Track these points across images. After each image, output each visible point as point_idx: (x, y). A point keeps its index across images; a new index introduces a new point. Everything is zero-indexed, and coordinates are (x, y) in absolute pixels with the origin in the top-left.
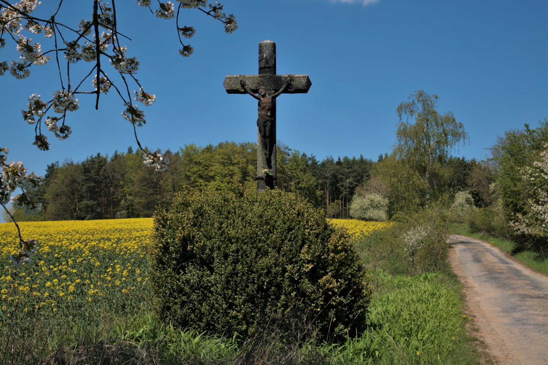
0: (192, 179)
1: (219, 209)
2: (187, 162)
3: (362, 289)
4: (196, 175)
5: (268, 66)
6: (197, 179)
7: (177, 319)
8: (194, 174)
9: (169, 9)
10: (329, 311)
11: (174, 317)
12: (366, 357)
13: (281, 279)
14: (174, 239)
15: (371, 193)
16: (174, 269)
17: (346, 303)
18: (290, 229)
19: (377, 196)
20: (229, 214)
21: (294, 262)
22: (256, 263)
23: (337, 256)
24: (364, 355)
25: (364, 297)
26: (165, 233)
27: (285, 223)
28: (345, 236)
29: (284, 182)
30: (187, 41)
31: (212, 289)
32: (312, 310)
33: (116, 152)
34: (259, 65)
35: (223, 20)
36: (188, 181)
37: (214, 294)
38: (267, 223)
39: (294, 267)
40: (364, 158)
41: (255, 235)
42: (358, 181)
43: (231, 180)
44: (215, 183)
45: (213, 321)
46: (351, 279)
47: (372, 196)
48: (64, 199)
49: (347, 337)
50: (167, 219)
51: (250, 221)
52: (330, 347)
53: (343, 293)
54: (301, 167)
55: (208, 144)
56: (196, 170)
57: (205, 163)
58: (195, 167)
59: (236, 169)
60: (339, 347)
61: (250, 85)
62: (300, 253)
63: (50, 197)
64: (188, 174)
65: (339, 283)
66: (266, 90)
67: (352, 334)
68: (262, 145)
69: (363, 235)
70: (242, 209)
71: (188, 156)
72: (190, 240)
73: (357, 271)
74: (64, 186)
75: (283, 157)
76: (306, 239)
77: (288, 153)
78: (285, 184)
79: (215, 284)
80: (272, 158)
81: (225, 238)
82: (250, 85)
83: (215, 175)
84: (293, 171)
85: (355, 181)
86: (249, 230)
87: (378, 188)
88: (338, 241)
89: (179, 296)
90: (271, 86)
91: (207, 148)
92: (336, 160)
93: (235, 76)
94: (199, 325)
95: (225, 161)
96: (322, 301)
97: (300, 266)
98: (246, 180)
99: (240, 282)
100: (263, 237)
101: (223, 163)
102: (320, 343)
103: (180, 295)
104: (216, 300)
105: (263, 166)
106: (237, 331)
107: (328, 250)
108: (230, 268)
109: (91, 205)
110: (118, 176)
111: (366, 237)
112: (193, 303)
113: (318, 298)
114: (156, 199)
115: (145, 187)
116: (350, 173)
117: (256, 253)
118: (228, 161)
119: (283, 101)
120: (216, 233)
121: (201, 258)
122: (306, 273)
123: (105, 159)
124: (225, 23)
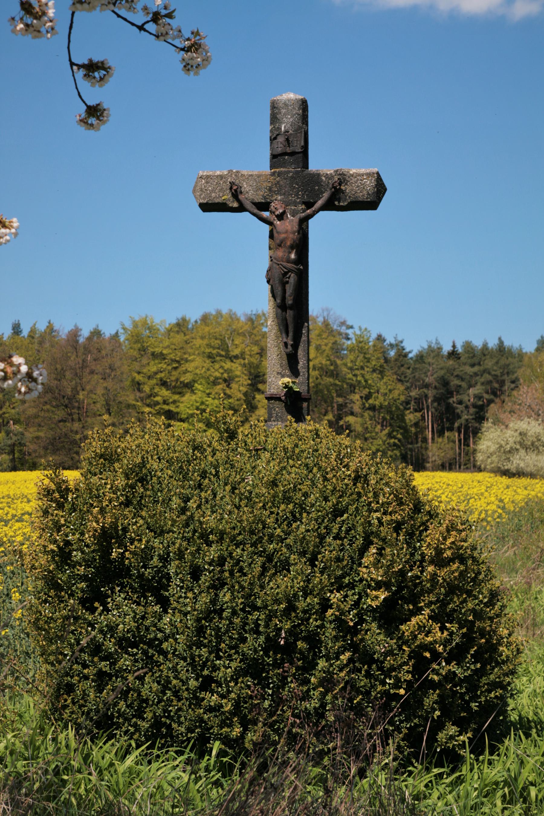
0: (147, 389)
1: (181, 467)
2: (135, 353)
3: (499, 643)
4: (154, 381)
5: (291, 150)
7: (88, 713)
8: (149, 378)
9: (44, 13)
10: (425, 694)
11: (81, 706)
12: (508, 801)
13: (319, 623)
14: (82, 534)
15: (520, 419)
16: (83, 602)
17: (462, 676)
18: (337, 512)
19: (533, 423)
20: (204, 478)
21: (347, 585)
22: (262, 587)
23: (443, 573)
24: (504, 796)
25: (504, 662)
26: (62, 521)
27: (326, 499)
28: (460, 527)
29: (339, 396)
30: (94, 94)
31: (165, 645)
32: (386, 693)
34: (272, 149)
35: (177, 42)
36: (138, 394)
37: (170, 656)
38: (287, 499)
39: (346, 596)
40: (507, 343)
41: (260, 526)
42: (494, 394)
44: (194, 397)
45: (167, 717)
46: (473, 623)
47: (523, 425)
49: (466, 753)
50: (68, 490)
51: (251, 493)
52: (427, 778)
53: (457, 655)
54: (374, 363)
55: (180, 316)
56: (154, 369)
59: (237, 368)
60: (449, 775)
61: (250, 193)
62: (360, 565)
64: (138, 378)
65: (446, 633)
66: (287, 204)
67: (477, 749)
68: (279, 325)
69: (503, 508)
70: (232, 466)
71: (137, 342)
72: (118, 537)
73: (486, 605)
75: (335, 343)
76: (372, 533)
77: (347, 334)
78: (340, 400)
79: (173, 636)
80: (301, 353)
81: (195, 531)
82: (250, 193)
83: (194, 381)
84: (358, 372)
85: (487, 392)
86: (247, 515)
87: (536, 408)
88: (445, 539)
89: (92, 661)
90: (297, 195)
91: (178, 325)
92: (447, 348)
93: (218, 173)
94: (135, 725)
96: (408, 672)
97: (359, 594)
99: (227, 631)
100: (279, 530)
101: (210, 356)
102: (405, 767)
103: (96, 659)
104: (174, 669)
105: (280, 370)
106: (220, 739)
107: (423, 560)
108: (205, 599)
111: (508, 513)
112: (122, 677)
113: (401, 666)
114: (72, 431)
115: (48, 407)
116: (476, 374)
117: (263, 566)
118: (220, 352)
119: (325, 228)
120: (174, 521)
121: (141, 576)
122: (373, 610)
124: (182, 49)
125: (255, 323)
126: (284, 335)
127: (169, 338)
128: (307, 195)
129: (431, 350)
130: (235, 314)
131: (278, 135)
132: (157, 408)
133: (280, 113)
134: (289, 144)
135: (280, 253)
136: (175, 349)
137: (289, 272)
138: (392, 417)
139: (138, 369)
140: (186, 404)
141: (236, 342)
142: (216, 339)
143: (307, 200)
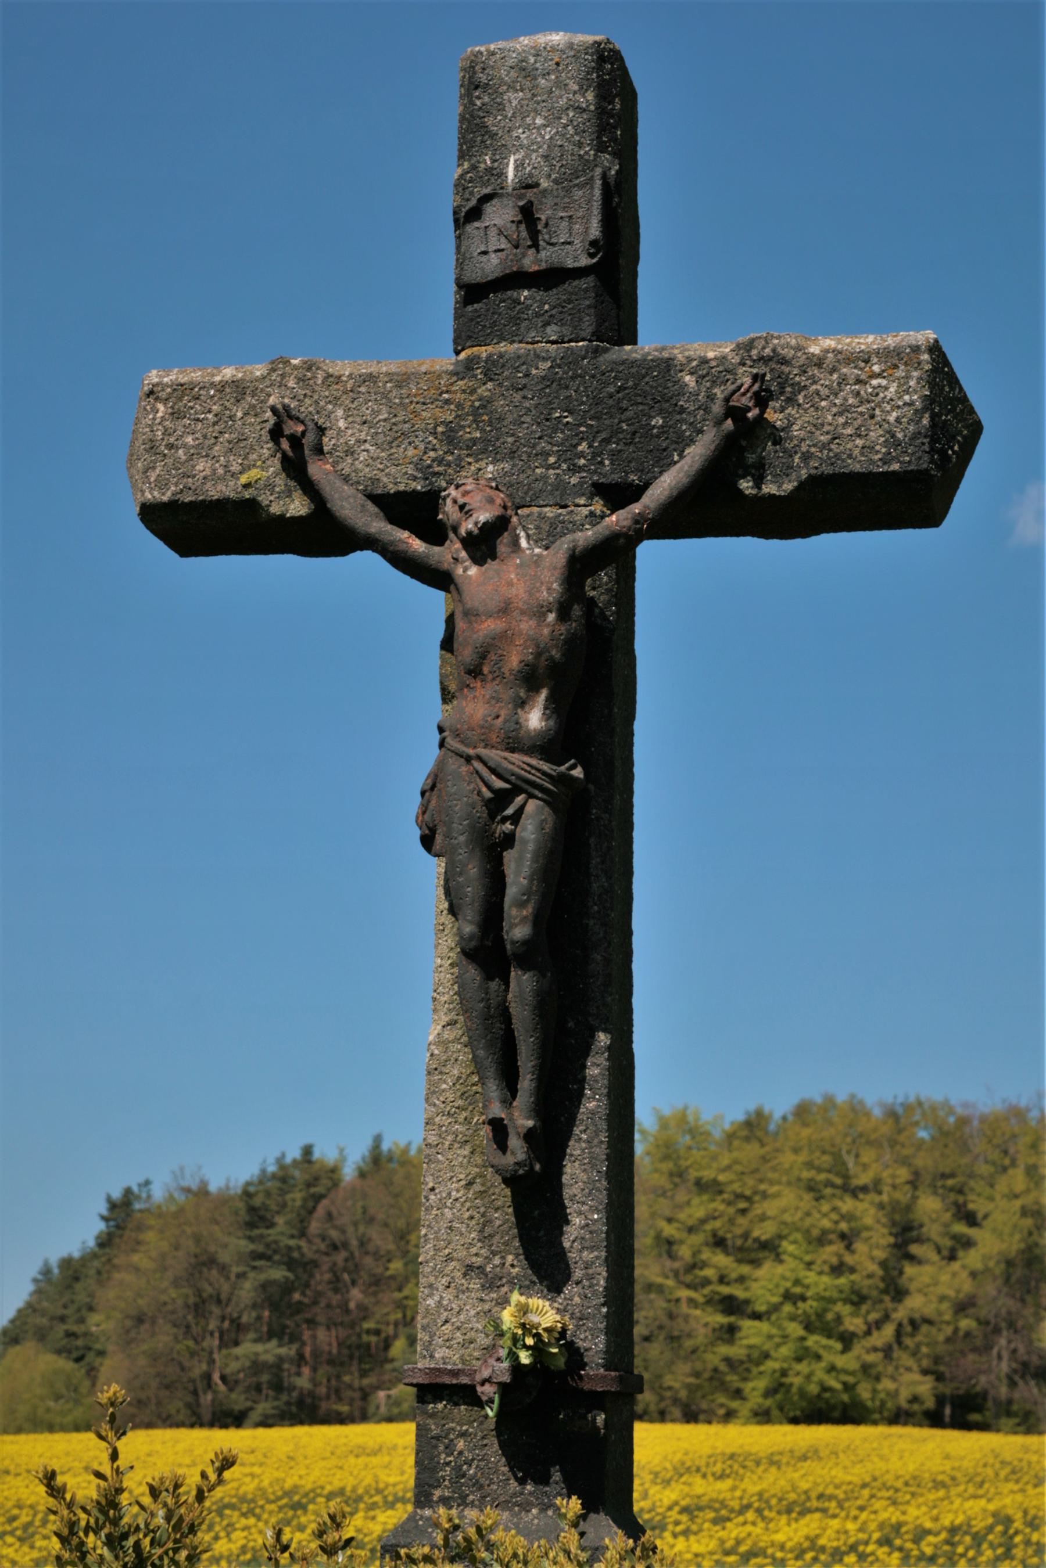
0: (685, 1252)
2: (662, 1181)
5: (564, 276)
6: (706, 1255)
8: (691, 1230)
33: (378, 1140)
36: (668, 1263)
43: (849, 1259)
44: (780, 1269)
48: (164, 1337)
55: (752, 1107)
56: (700, 1213)
57: (736, 1187)
58: (696, 1201)
61: (361, 457)
63: (109, 1326)
64: (669, 1230)
71: (666, 1157)
74: (165, 1284)
82: (361, 457)
83: (781, 1237)
90: (568, 453)
95: (822, 1177)
98: (911, 1258)
101: (811, 1187)
109: (270, 1358)
110: (382, 1240)
123: (334, 1171)
125: (903, 1121)
126: (494, 1089)
127: (730, 1151)
128: (613, 454)
130: (861, 1103)
131: (487, 198)
132: (706, 1291)
133: (501, 107)
134: (534, 234)
135: (477, 707)
136: (743, 1173)
137: (516, 790)
139: (667, 1213)
140: (764, 1283)
141: (864, 1159)
142: (824, 1152)
143: (616, 478)
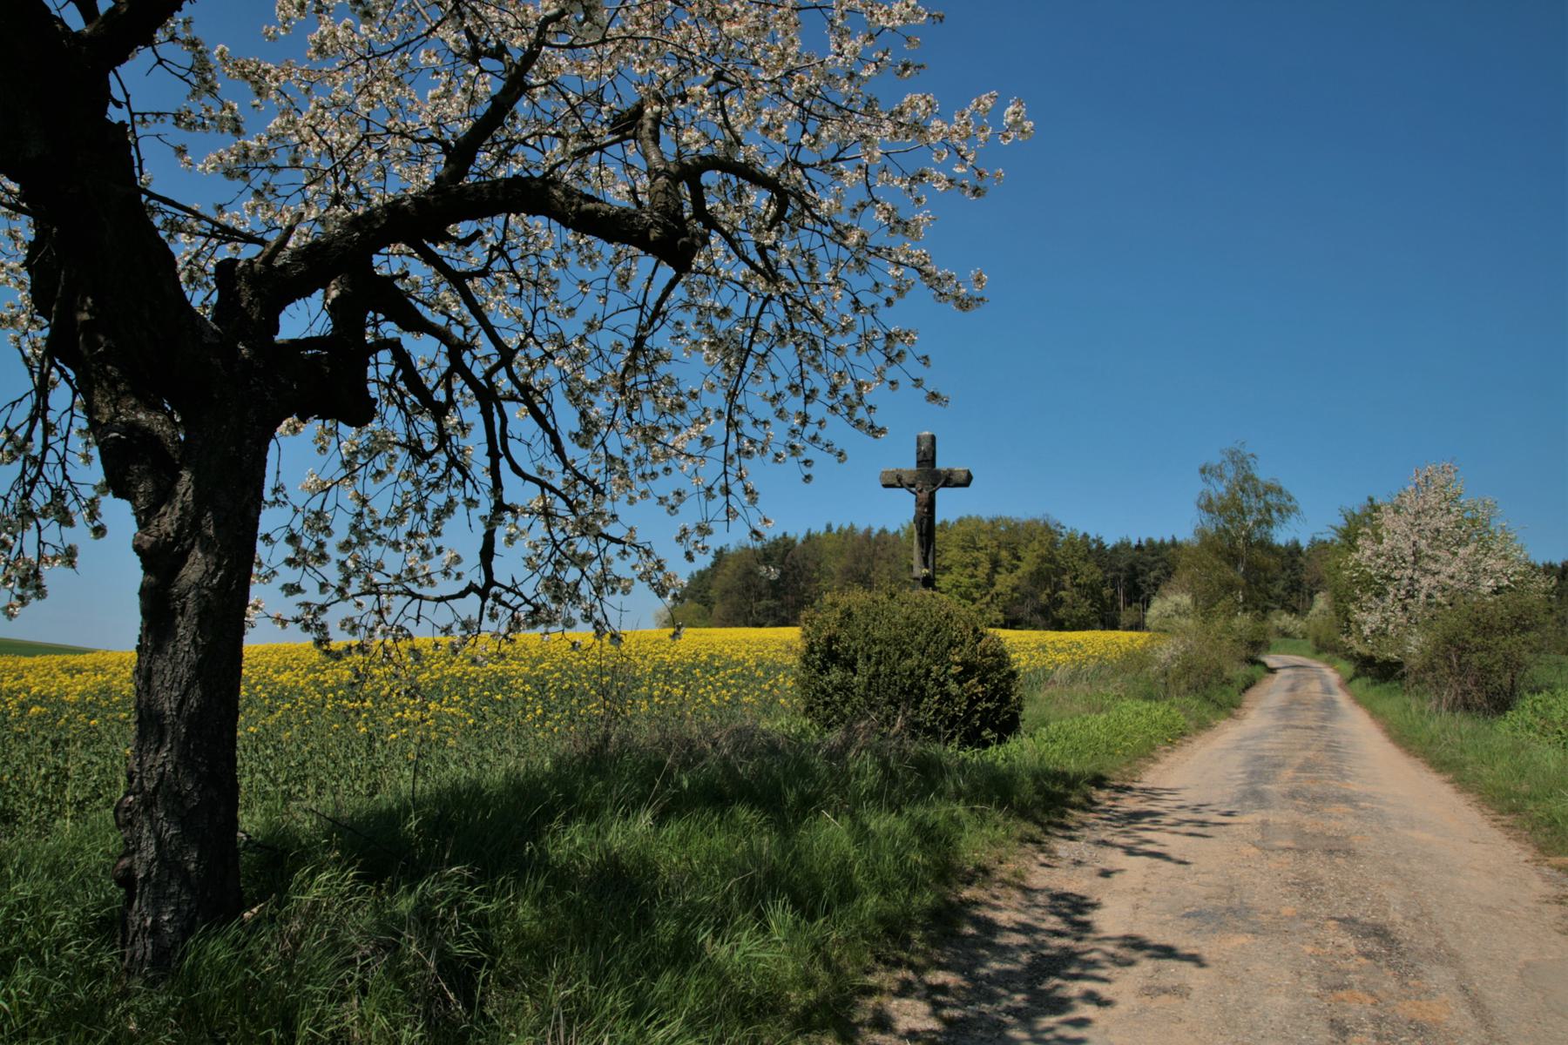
5: (927, 457)
18: (936, 631)
40: (1178, 539)
47: (1177, 598)
48: (735, 598)
61: (906, 479)
82: (906, 479)
86: (893, 632)
92: (1134, 543)
110: (811, 566)
123: (794, 541)
129: (1122, 544)
138: (1092, 591)
